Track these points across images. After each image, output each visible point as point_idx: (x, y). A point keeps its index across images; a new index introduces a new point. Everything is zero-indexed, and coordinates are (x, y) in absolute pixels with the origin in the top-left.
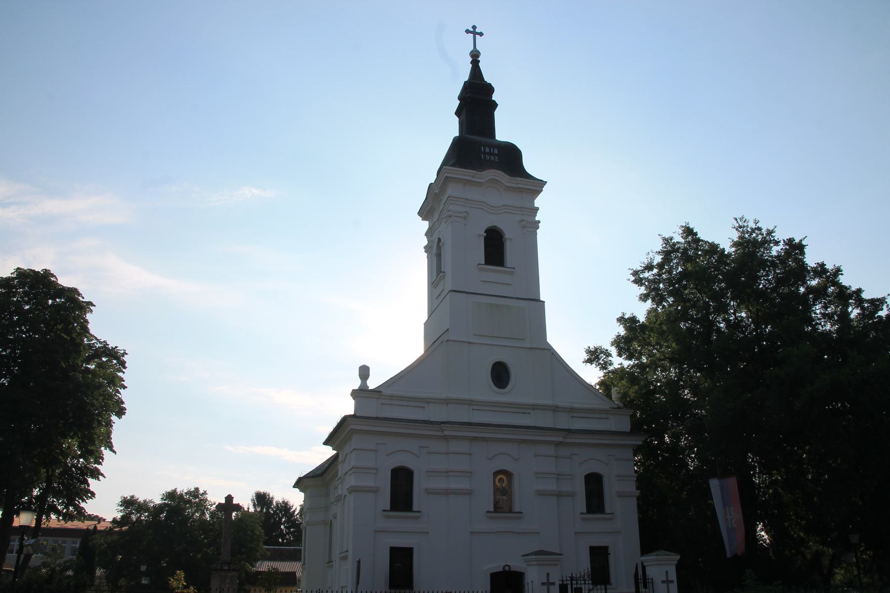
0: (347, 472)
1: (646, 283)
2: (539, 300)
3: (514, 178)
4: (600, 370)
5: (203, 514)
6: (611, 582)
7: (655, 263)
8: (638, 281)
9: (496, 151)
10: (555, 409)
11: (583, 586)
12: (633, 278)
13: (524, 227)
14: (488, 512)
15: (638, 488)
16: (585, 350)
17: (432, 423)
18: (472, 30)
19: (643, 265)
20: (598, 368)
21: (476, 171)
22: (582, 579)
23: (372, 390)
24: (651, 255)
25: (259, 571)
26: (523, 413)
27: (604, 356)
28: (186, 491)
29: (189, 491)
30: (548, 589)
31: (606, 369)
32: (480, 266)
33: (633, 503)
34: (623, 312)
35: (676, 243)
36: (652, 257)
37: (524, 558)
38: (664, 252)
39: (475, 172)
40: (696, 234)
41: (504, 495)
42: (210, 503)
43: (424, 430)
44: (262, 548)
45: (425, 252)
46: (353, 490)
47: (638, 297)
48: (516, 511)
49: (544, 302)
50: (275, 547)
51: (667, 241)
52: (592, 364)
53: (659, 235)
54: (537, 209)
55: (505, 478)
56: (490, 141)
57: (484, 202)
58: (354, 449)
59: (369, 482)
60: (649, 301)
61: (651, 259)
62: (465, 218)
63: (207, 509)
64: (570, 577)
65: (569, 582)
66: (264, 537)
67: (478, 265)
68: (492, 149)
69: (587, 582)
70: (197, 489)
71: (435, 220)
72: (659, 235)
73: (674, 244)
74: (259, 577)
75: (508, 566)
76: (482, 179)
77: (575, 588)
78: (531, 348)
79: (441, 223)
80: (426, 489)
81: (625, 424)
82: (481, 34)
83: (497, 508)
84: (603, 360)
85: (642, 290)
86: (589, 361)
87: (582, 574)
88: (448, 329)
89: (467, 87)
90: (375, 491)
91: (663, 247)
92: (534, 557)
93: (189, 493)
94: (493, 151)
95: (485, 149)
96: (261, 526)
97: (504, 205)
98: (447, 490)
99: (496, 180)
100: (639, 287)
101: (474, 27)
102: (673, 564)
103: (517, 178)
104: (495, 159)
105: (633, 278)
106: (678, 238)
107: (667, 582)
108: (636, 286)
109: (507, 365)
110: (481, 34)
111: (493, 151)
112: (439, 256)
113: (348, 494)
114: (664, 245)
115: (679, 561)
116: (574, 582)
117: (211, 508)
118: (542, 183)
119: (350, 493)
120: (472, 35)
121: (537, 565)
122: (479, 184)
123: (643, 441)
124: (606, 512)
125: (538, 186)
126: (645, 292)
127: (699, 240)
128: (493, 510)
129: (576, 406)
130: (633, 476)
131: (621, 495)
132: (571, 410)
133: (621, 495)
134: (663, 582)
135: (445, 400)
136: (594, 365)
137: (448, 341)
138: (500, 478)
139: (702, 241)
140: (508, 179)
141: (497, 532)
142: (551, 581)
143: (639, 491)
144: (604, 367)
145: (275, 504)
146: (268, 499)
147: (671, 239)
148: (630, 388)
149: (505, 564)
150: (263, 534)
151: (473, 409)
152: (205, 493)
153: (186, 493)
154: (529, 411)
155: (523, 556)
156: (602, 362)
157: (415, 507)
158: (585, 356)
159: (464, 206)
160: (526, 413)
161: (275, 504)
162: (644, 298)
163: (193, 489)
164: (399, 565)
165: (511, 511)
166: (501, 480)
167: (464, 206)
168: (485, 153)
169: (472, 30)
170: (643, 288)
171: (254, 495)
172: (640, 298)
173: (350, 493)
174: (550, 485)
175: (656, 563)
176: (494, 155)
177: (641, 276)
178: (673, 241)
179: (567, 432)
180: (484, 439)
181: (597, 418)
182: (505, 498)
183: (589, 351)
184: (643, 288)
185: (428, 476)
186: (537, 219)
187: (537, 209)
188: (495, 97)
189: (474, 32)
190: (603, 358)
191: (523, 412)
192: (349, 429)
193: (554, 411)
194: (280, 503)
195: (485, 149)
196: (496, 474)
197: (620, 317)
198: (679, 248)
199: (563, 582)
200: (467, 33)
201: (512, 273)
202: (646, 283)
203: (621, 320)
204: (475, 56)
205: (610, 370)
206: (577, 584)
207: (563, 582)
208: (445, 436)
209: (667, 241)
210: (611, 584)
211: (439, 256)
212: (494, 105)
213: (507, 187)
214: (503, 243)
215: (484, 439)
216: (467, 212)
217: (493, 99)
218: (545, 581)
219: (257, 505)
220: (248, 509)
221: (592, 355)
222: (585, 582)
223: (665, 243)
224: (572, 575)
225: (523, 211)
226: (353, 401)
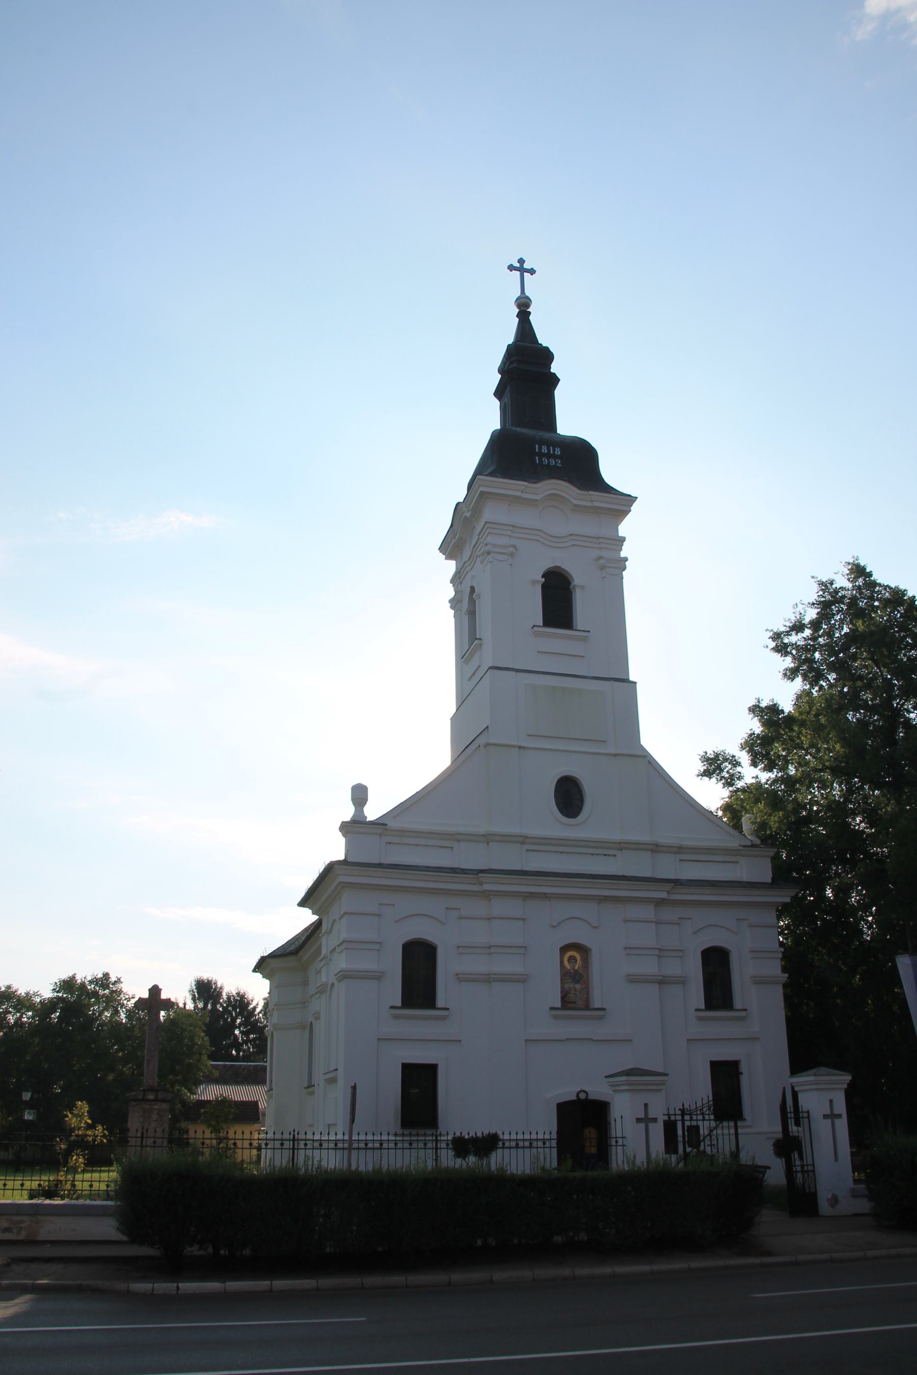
0: (334, 949)
1: (794, 652)
2: (626, 681)
3: (586, 493)
4: (724, 787)
5: (116, 1012)
6: (744, 1117)
7: (807, 620)
8: (782, 649)
9: (558, 452)
10: (656, 849)
11: (700, 1123)
12: (772, 644)
13: (602, 568)
14: (552, 1008)
15: (784, 970)
16: (700, 757)
17: (464, 871)
18: (518, 265)
19: (788, 624)
20: (720, 784)
22: (699, 1112)
23: (372, 823)
24: (800, 608)
25: (202, 1100)
26: (605, 855)
27: (730, 766)
28: (89, 978)
29: (95, 978)
31: (732, 785)
32: (535, 629)
33: (777, 995)
34: (757, 697)
35: (840, 589)
36: (802, 612)
37: (611, 1080)
38: (821, 602)
39: (526, 483)
40: (870, 575)
41: (578, 982)
42: (127, 997)
44: (206, 1065)
45: (451, 607)
46: (345, 976)
47: (781, 674)
48: (596, 1006)
49: (636, 683)
50: (226, 1063)
51: (825, 586)
52: (710, 778)
53: (813, 577)
54: (623, 540)
55: (578, 956)
56: (547, 435)
58: (346, 913)
59: (366, 963)
60: (799, 680)
61: (801, 614)
62: (512, 555)
63: (122, 1005)
64: (680, 1109)
65: (679, 1118)
66: (209, 1047)
67: (533, 628)
68: (551, 448)
69: (707, 1117)
70: (106, 976)
71: (465, 558)
72: (813, 577)
73: (836, 591)
74: (202, 1110)
75: (585, 1092)
76: (537, 494)
77: (688, 1126)
78: (616, 755)
79: (475, 563)
80: (457, 975)
81: (762, 871)
82: (532, 272)
83: (567, 1002)
84: (728, 772)
85: (788, 662)
86: (707, 774)
87: (699, 1104)
88: (488, 727)
89: (513, 353)
90: (378, 977)
91: (818, 596)
92: (624, 1078)
93: (94, 981)
94: (554, 451)
95: (540, 448)
96: (203, 1031)
97: (571, 535)
98: (488, 975)
100: (783, 658)
101: (521, 261)
103: (591, 492)
104: (556, 463)
105: (772, 644)
106: (842, 582)
107: (832, 1116)
108: (777, 656)
110: (532, 272)
111: (554, 451)
112: (472, 613)
113: (336, 982)
114: (821, 593)
115: (850, 1084)
116: (687, 1117)
117: (128, 1003)
118: (629, 500)
119: (339, 981)
120: (519, 272)
121: (817, 1089)
122: (533, 503)
123: (792, 897)
125: (623, 503)
126: (792, 665)
127: (874, 584)
128: (560, 1006)
129: (684, 843)
131: (759, 981)
132: (679, 850)
133: (759, 981)
134: (825, 1117)
135: (484, 835)
136: (714, 780)
137: (487, 745)
138: (570, 956)
139: (880, 585)
140: (578, 494)
141: (567, 1039)
142: (650, 1116)
143: (787, 975)
144: (729, 782)
145: (225, 997)
146: (215, 989)
147: (831, 583)
148: (770, 815)
149: (580, 1090)
150: (208, 1043)
151: (527, 850)
152: (118, 981)
153: (89, 981)
155: (606, 1077)
156: (727, 775)
157: (440, 1003)
158: (701, 767)
159: (510, 536)
160: (609, 855)
161: (225, 997)
162: (791, 674)
163: (100, 975)
164: (416, 1091)
165: (587, 1007)
166: (572, 959)
167: (510, 536)
168: (541, 455)
169: (518, 265)
170: (789, 659)
171: (194, 983)
172: (785, 675)
173: (339, 981)
174: (649, 967)
175: (814, 1087)
176: (554, 456)
177: (786, 641)
178: (834, 586)
179: (673, 884)
180: (545, 896)
182: (578, 986)
183: (706, 759)
184: (789, 659)
185: (460, 954)
186: (623, 554)
187: (623, 540)
188: (555, 368)
189: (521, 268)
190: (727, 769)
191: (561, 851)
192: (336, 883)
193: (653, 851)
194: (233, 996)
195: (540, 448)
196: (564, 949)
197: (753, 706)
198: (844, 597)
199: (669, 1117)
201: (585, 639)
202: (794, 652)
203: (756, 710)
205: (739, 787)
206: (691, 1119)
207: (669, 1117)
208: (485, 891)
209: (826, 586)
210: (745, 1120)
211: (472, 613)
212: (554, 381)
213: (576, 506)
214: (571, 593)
215: (545, 896)
216: (514, 546)
217: (552, 371)
218: (828, 1112)
219: (198, 999)
220: (185, 1004)
221: (710, 764)
222: (704, 1117)
223: (822, 590)
224: (683, 1105)
225: (600, 543)
226: (344, 839)
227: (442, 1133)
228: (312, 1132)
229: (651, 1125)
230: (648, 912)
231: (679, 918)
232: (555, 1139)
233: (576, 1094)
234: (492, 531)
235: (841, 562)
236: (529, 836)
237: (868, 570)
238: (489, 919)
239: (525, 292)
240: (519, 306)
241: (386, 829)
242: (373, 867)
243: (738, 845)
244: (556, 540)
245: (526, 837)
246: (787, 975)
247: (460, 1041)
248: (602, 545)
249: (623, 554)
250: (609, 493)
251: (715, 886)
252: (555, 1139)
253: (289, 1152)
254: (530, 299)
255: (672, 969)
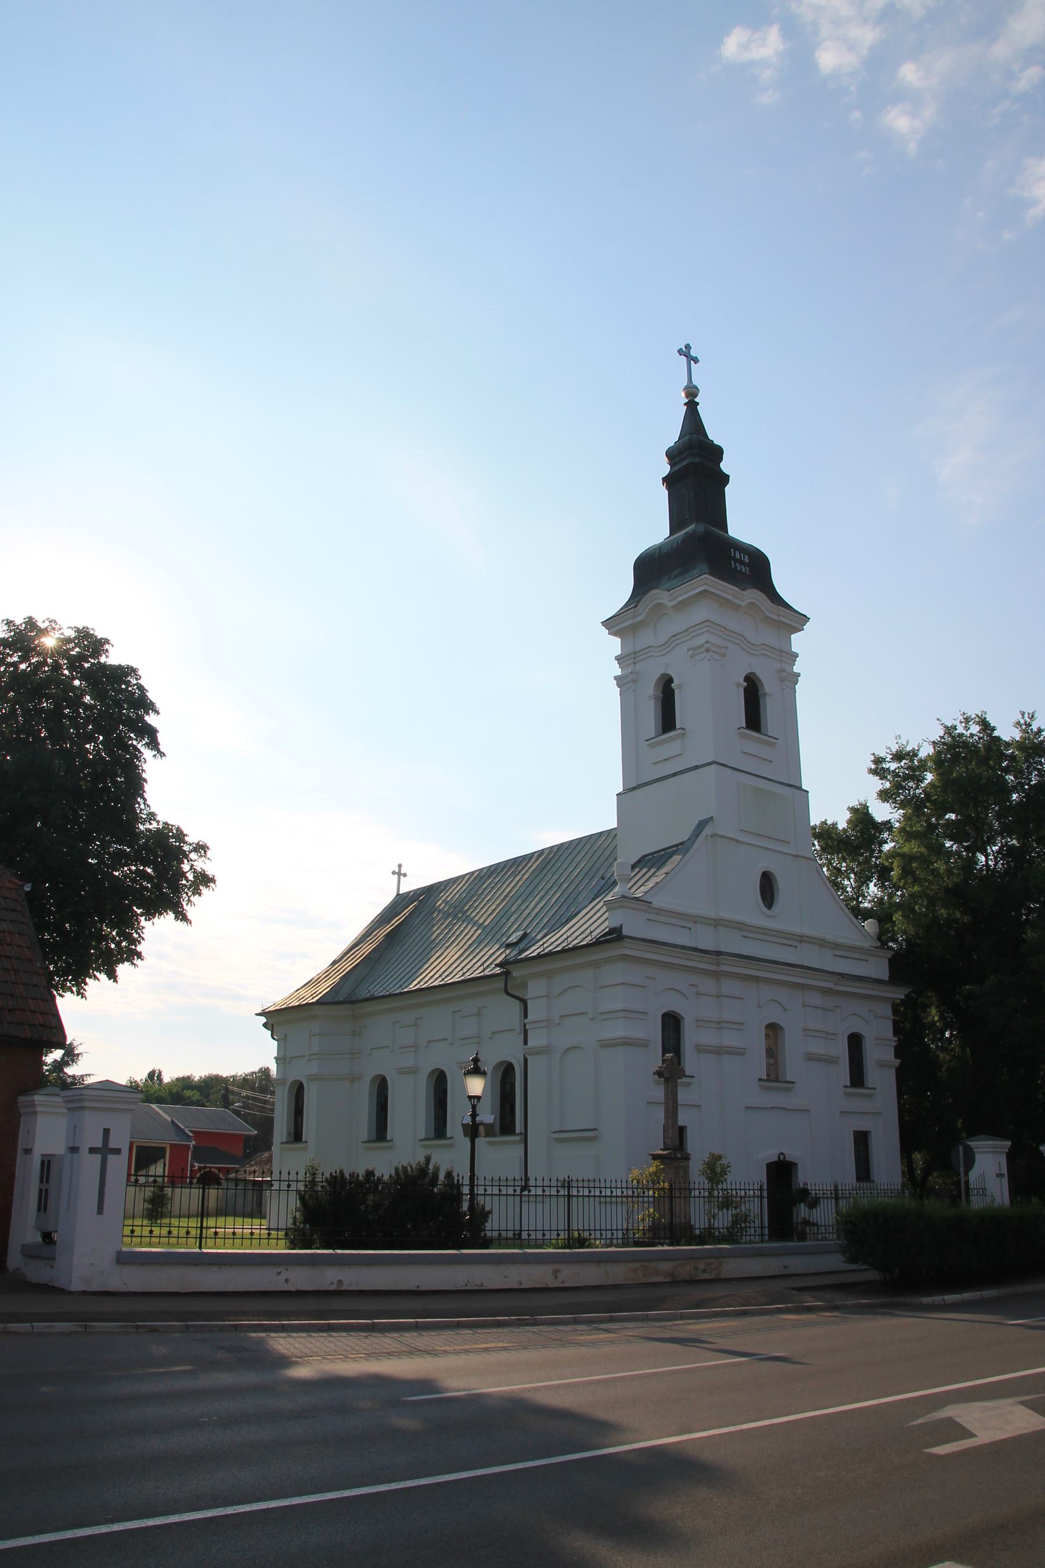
2: (800, 788)
14: (760, 1080)
15: (897, 1056)
21: (740, 589)
26: (790, 946)
30: (280, 1188)
39: (737, 589)
43: (757, 970)
54: (796, 655)
57: (743, 636)
62: (724, 655)
68: (742, 555)
72: (938, 719)
78: (797, 856)
81: (878, 968)
99: (758, 607)
102: (1002, 1152)
103: (780, 607)
109: (776, 881)
115: (1011, 1149)
118: (804, 619)
121: (993, 1152)
124: (866, 1086)
125: (799, 621)
129: (839, 941)
130: (891, 1040)
131: (881, 1064)
133: (881, 1064)
135: (715, 920)
137: (713, 836)
140: (771, 607)
142: (111, 1145)
143: (899, 1061)
154: (795, 943)
175: (992, 1150)
181: (856, 959)
185: (698, 1027)
186: (796, 669)
188: (725, 466)
191: (789, 944)
200: (680, 355)
201: (773, 745)
204: (692, 393)
212: (725, 479)
213: (768, 617)
218: (99, 1144)
227: (573, 1179)
228: (534, 1178)
229: (111, 1158)
230: (815, 999)
231: (834, 1006)
232: (467, 1185)
233: (777, 1155)
234: (710, 629)
235: (960, 711)
236: (746, 923)
237: (1007, 732)
238: (717, 997)
239: (693, 381)
240: (687, 396)
241: (650, 907)
242: (641, 941)
243: (868, 945)
244: (749, 645)
245: (744, 924)
246: (899, 1061)
247: (808, 1111)
248: (784, 659)
249: (796, 669)
250: (790, 610)
251: (862, 980)
252: (467, 1185)
253: (564, 1200)
254: (698, 389)
255: (731, 1040)
